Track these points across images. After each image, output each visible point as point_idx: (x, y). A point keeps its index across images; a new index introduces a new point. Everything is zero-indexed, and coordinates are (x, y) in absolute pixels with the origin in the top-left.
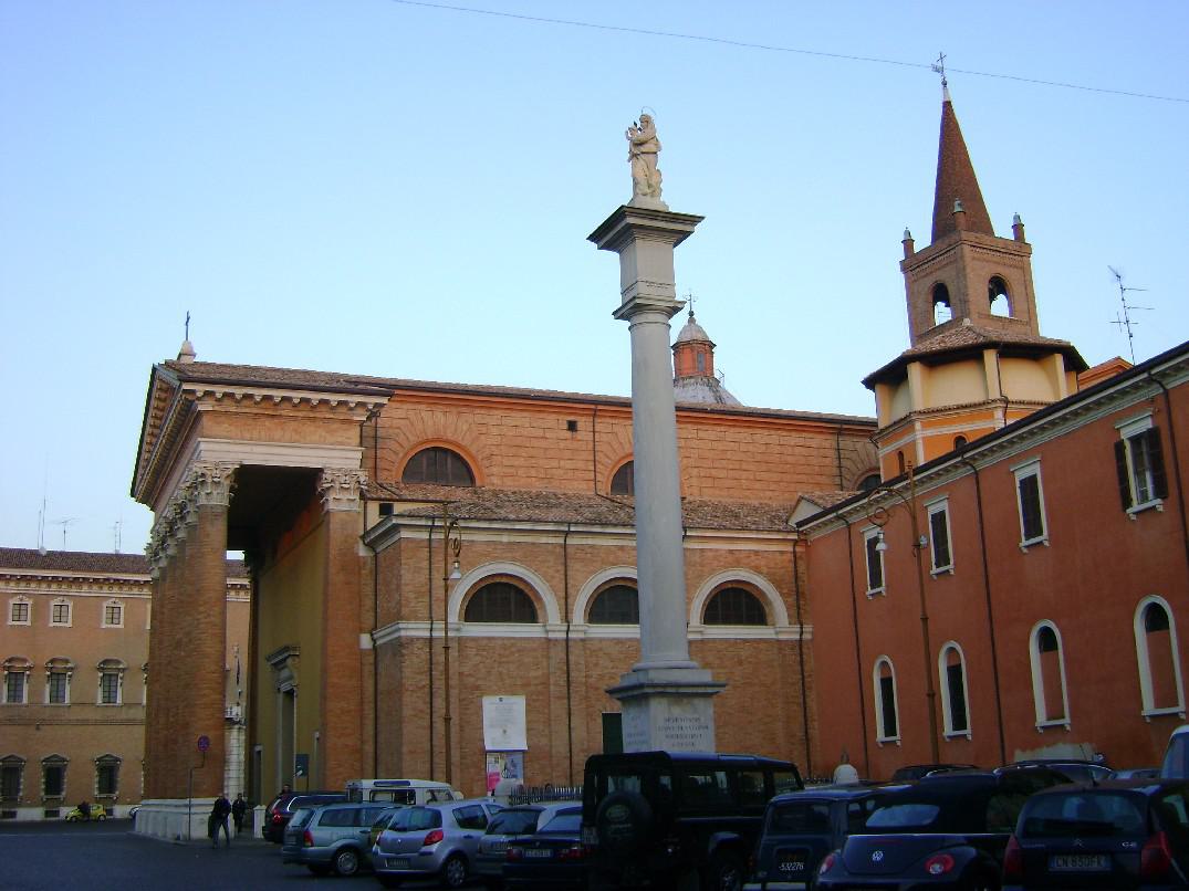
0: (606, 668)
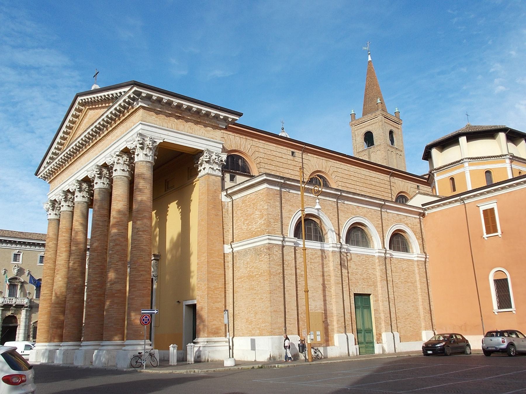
0: (354, 269)
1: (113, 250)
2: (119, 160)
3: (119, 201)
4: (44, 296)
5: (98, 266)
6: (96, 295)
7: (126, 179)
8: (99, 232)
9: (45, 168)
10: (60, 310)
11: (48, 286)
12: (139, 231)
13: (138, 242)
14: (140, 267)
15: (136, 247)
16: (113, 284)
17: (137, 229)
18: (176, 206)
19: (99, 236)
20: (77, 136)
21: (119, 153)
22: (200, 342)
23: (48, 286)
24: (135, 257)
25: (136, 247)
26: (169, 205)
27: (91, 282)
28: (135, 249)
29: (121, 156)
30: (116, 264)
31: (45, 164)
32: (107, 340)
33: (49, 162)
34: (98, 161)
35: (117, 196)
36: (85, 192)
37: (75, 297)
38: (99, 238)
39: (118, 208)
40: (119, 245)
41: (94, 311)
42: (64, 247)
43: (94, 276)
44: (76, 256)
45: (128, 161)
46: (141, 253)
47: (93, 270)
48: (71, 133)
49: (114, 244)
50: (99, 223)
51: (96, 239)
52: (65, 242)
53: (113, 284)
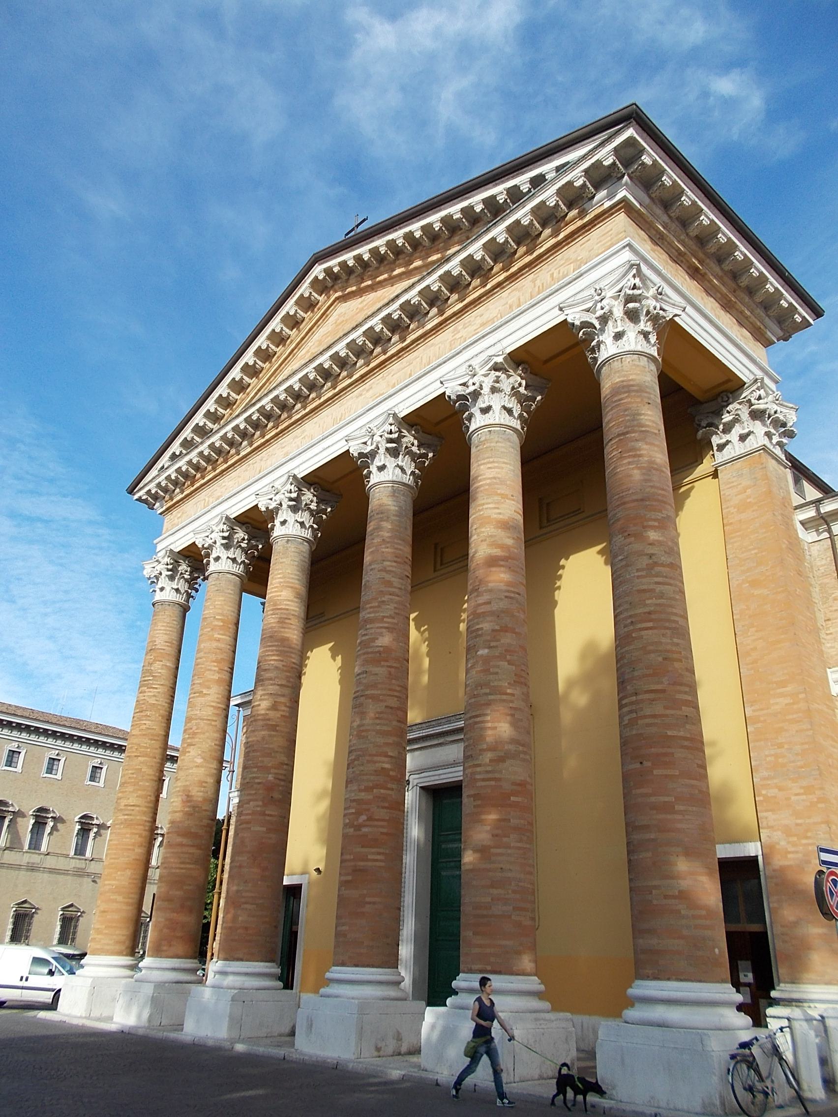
1: (493, 647)
2: (497, 381)
3: (504, 496)
4: (127, 812)
5: (391, 708)
6: (386, 805)
7: (515, 438)
8: (392, 606)
9: (174, 457)
11: (140, 783)
12: (656, 564)
13: (659, 601)
14: (678, 688)
15: (653, 616)
16: (501, 759)
17: (651, 556)
18: (329, 654)
19: (393, 618)
20: (286, 372)
21: (505, 359)
22: (812, 1001)
23: (140, 783)
24: (654, 652)
25: (653, 616)
26: (309, 654)
27: (368, 758)
28: (650, 624)
29: (505, 371)
30: (509, 691)
33: (178, 453)
34: (172, 543)
35: (498, 481)
36: (239, 551)
37: (267, 812)
38: (392, 623)
39: (501, 516)
40: (513, 631)
41: (379, 857)
42: (216, 669)
43: (380, 740)
45: (246, 542)
46: (675, 640)
47: (378, 721)
48: (264, 371)
49: (497, 627)
50: (393, 579)
51: (386, 625)
52: (220, 657)
53: (501, 759)
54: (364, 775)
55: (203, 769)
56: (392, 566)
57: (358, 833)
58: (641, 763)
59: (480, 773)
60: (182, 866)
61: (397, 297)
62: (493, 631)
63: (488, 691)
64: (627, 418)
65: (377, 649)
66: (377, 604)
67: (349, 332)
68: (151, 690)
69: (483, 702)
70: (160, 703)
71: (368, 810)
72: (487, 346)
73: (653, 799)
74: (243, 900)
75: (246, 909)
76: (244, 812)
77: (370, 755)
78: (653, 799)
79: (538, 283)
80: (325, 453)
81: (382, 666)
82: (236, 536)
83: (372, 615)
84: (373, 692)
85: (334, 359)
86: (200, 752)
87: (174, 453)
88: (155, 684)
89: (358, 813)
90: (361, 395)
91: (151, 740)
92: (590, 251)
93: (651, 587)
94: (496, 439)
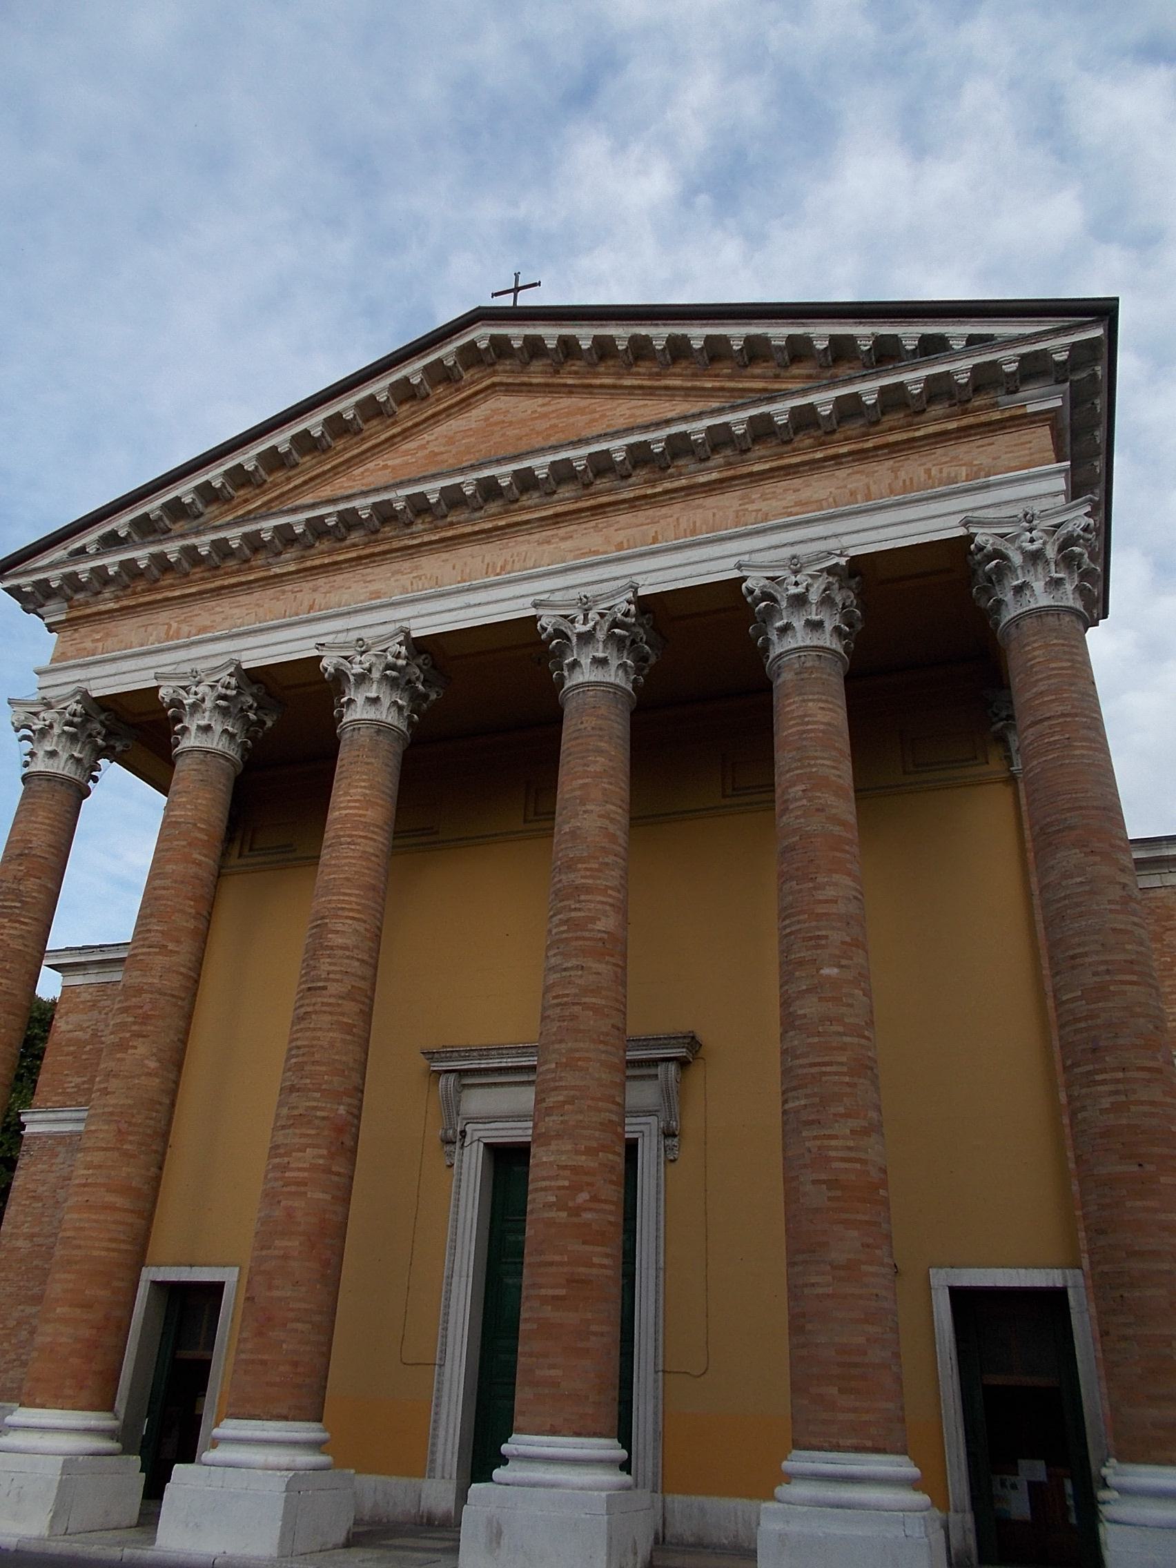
10: (131, 1225)
15: (1136, 968)
25: (1136, 968)
27: (590, 1102)
31: (90, 538)
32: (869, 1444)
42: (193, 911)
44: (357, 964)
49: (848, 939)
51: (610, 900)
54: (584, 1128)
55: (157, 1080)
56: (617, 813)
57: (576, 1220)
58: (1140, 1165)
59: (836, 1148)
60: (114, 1245)
61: (668, 422)
62: (843, 943)
63: (841, 1029)
64: (1075, 695)
65: (600, 935)
66: (596, 866)
67: (562, 446)
68: (17, 925)
69: (834, 1044)
70: (30, 950)
71: (592, 1185)
72: (814, 536)
73: (1163, 1217)
74: (291, 1315)
75: (296, 1331)
76: (292, 1165)
77: (593, 1099)
78: (1163, 1217)
79: (902, 474)
80: (462, 614)
81: (607, 963)
82: (243, 699)
83: (590, 881)
84: (594, 1000)
85: (517, 476)
86: (154, 1050)
87: (113, 533)
88: (25, 917)
89: (575, 1188)
90: (549, 542)
91: (9, 1013)
92: (994, 459)
93: (1129, 927)
94: (828, 670)
